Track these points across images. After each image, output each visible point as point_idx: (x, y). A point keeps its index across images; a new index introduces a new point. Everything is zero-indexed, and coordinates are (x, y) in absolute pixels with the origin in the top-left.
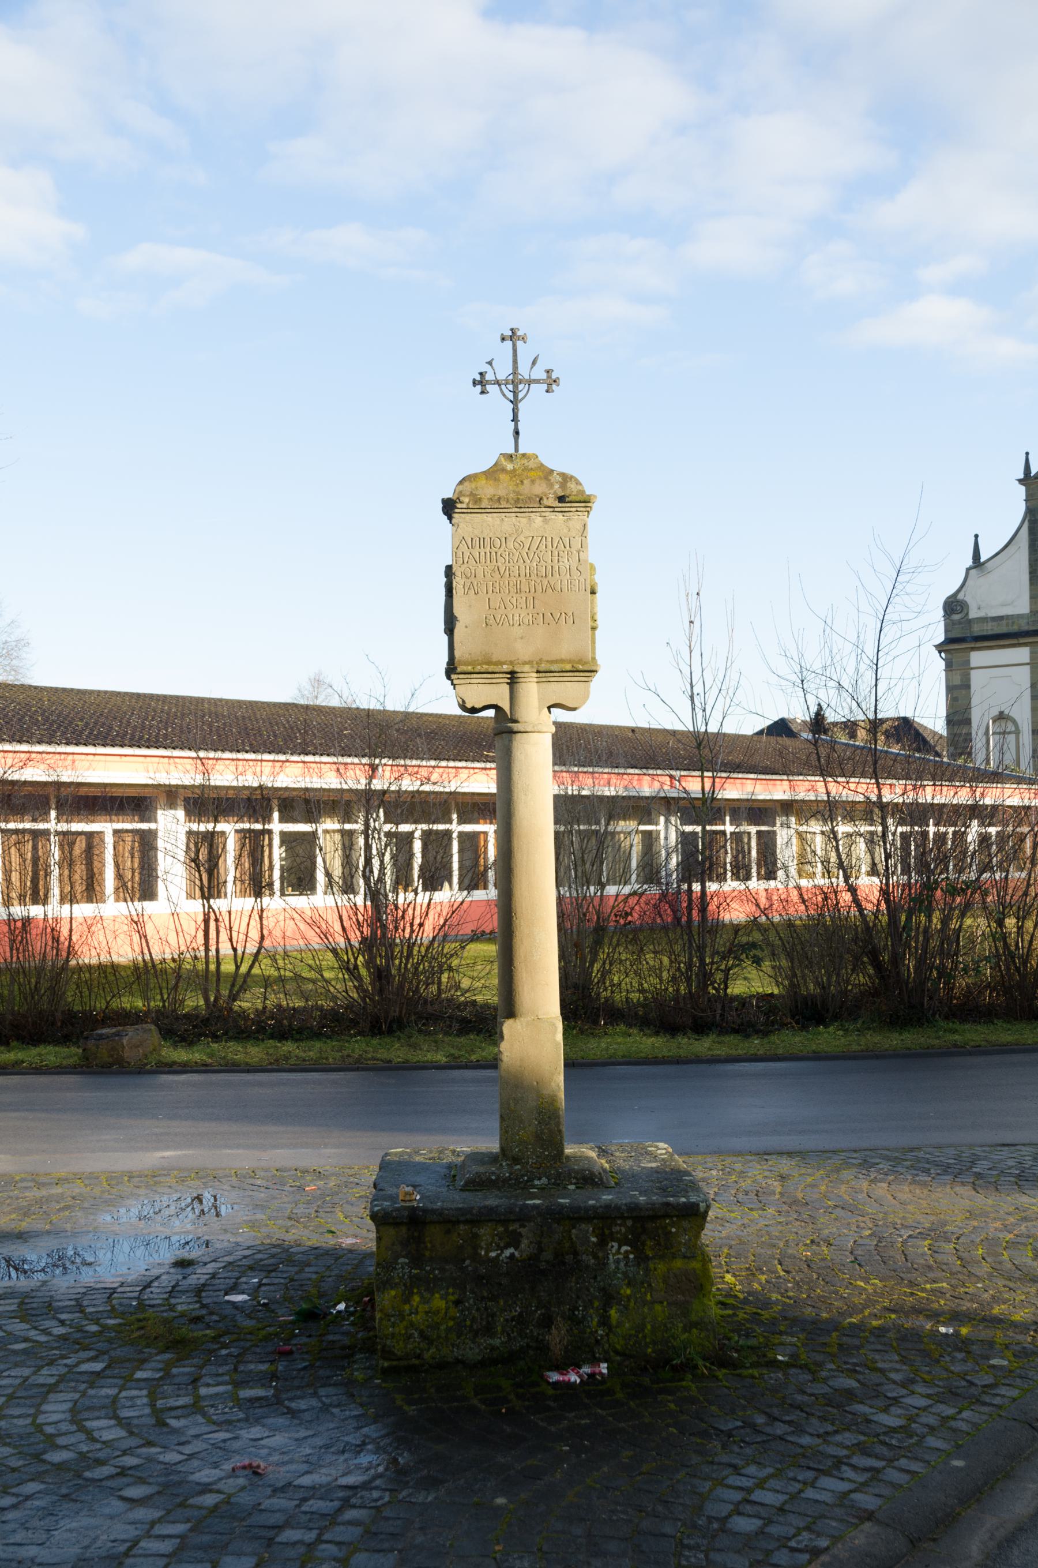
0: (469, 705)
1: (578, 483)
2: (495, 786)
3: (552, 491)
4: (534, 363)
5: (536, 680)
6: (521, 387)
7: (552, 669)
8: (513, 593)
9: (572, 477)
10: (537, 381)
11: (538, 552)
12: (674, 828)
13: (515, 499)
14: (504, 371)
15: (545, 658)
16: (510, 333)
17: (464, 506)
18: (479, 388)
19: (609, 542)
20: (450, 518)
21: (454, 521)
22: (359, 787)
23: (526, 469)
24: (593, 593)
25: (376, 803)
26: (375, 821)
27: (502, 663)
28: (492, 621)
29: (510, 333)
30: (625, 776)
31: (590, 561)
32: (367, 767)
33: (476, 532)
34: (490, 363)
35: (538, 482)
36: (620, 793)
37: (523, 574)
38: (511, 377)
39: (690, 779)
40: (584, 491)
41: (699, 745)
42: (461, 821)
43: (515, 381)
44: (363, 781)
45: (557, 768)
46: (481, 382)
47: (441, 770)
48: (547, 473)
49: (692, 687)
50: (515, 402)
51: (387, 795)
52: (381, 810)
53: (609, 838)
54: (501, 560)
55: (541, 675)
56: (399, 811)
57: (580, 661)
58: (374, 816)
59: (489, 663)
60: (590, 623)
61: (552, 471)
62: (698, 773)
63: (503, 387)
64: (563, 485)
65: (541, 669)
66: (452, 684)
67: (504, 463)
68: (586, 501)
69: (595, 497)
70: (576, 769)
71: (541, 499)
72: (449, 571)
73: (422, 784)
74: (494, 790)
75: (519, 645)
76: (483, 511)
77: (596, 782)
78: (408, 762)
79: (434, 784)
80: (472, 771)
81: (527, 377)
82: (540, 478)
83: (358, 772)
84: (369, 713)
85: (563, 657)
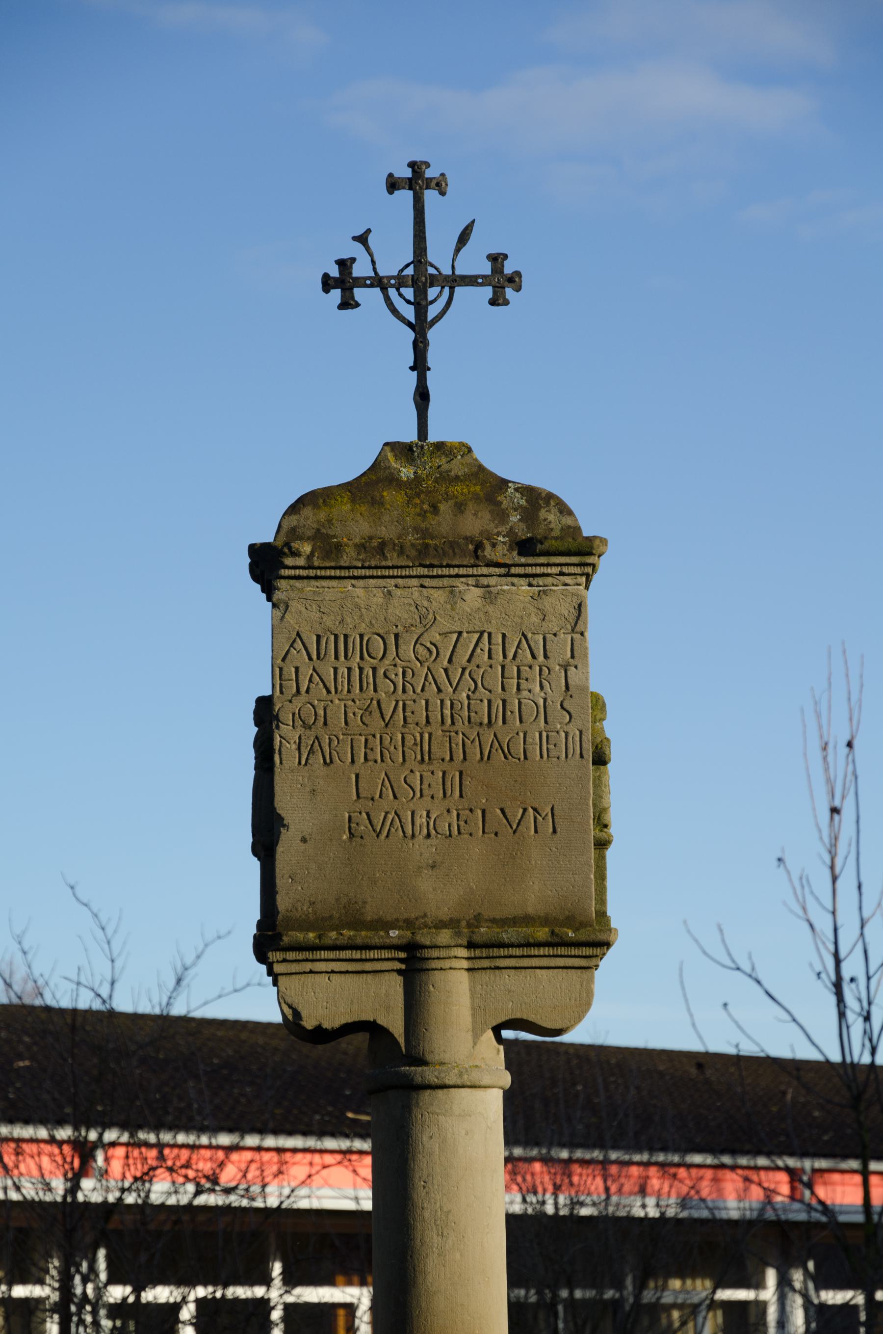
0: (309, 1023)
1: (564, 510)
2: (369, 1193)
3: (504, 529)
4: (464, 238)
5: (465, 964)
6: (432, 292)
7: (505, 937)
8: (411, 763)
9: (550, 496)
10: (470, 281)
11: (471, 667)
12: (799, 1300)
13: (419, 583)
14: (395, 256)
15: (487, 914)
16: (408, 173)
17: (301, 562)
18: (336, 295)
19: (632, 643)
20: (268, 590)
21: (278, 595)
22: (48, 1198)
23: (445, 478)
24: (600, 759)
25: (89, 1239)
26: (85, 1280)
27: (386, 925)
28: (364, 827)
29: (408, 173)
30: (682, 1172)
31: (593, 688)
32: (66, 1149)
33: (328, 621)
34: (362, 239)
35: (471, 506)
36: (671, 1213)
37: (436, 716)
38: (410, 271)
39: (836, 1177)
40: (578, 529)
41: (857, 1099)
42: (291, 1280)
43: (420, 279)
44: (59, 1185)
45: (518, 1152)
46: (342, 283)
47: (248, 1155)
48: (494, 487)
49: (838, 962)
50: (420, 327)
51: (116, 1217)
52: (102, 1253)
53: (645, 1322)
54: (386, 686)
55: (478, 953)
56: (143, 1258)
57: (570, 921)
58: (85, 1266)
59: (357, 924)
60: (592, 832)
61: (505, 483)
62: (854, 1164)
63: (392, 292)
64: (530, 514)
65: (477, 939)
66: (270, 973)
67: (394, 464)
68: (582, 552)
69: (604, 542)
70: (564, 1154)
71: (479, 546)
72: (265, 711)
73: (198, 1192)
74: (367, 1205)
75: (426, 884)
76: (347, 573)
77: (613, 1188)
78: (166, 1137)
79: (228, 1191)
80: (317, 1158)
81: (447, 271)
82: (476, 498)
83: (45, 1161)
84: (74, 1018)
85: (530, 910)
